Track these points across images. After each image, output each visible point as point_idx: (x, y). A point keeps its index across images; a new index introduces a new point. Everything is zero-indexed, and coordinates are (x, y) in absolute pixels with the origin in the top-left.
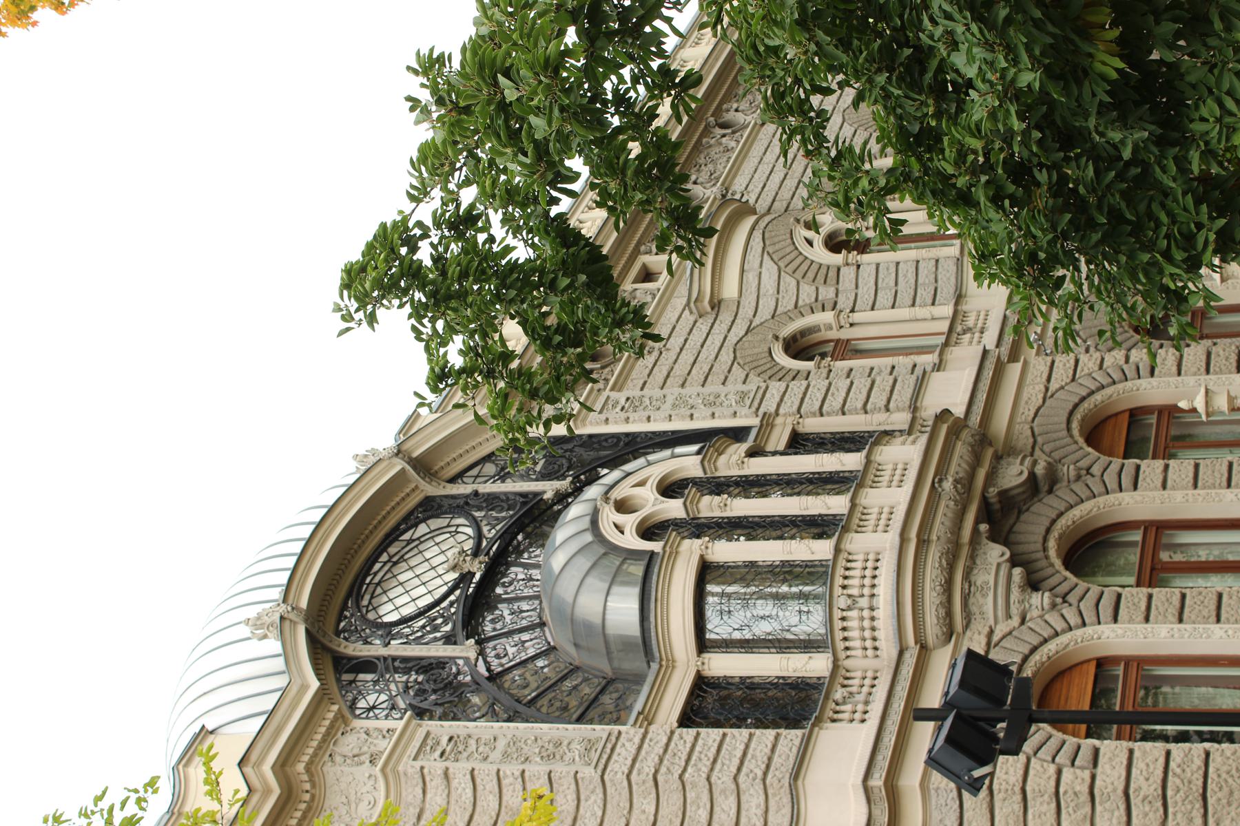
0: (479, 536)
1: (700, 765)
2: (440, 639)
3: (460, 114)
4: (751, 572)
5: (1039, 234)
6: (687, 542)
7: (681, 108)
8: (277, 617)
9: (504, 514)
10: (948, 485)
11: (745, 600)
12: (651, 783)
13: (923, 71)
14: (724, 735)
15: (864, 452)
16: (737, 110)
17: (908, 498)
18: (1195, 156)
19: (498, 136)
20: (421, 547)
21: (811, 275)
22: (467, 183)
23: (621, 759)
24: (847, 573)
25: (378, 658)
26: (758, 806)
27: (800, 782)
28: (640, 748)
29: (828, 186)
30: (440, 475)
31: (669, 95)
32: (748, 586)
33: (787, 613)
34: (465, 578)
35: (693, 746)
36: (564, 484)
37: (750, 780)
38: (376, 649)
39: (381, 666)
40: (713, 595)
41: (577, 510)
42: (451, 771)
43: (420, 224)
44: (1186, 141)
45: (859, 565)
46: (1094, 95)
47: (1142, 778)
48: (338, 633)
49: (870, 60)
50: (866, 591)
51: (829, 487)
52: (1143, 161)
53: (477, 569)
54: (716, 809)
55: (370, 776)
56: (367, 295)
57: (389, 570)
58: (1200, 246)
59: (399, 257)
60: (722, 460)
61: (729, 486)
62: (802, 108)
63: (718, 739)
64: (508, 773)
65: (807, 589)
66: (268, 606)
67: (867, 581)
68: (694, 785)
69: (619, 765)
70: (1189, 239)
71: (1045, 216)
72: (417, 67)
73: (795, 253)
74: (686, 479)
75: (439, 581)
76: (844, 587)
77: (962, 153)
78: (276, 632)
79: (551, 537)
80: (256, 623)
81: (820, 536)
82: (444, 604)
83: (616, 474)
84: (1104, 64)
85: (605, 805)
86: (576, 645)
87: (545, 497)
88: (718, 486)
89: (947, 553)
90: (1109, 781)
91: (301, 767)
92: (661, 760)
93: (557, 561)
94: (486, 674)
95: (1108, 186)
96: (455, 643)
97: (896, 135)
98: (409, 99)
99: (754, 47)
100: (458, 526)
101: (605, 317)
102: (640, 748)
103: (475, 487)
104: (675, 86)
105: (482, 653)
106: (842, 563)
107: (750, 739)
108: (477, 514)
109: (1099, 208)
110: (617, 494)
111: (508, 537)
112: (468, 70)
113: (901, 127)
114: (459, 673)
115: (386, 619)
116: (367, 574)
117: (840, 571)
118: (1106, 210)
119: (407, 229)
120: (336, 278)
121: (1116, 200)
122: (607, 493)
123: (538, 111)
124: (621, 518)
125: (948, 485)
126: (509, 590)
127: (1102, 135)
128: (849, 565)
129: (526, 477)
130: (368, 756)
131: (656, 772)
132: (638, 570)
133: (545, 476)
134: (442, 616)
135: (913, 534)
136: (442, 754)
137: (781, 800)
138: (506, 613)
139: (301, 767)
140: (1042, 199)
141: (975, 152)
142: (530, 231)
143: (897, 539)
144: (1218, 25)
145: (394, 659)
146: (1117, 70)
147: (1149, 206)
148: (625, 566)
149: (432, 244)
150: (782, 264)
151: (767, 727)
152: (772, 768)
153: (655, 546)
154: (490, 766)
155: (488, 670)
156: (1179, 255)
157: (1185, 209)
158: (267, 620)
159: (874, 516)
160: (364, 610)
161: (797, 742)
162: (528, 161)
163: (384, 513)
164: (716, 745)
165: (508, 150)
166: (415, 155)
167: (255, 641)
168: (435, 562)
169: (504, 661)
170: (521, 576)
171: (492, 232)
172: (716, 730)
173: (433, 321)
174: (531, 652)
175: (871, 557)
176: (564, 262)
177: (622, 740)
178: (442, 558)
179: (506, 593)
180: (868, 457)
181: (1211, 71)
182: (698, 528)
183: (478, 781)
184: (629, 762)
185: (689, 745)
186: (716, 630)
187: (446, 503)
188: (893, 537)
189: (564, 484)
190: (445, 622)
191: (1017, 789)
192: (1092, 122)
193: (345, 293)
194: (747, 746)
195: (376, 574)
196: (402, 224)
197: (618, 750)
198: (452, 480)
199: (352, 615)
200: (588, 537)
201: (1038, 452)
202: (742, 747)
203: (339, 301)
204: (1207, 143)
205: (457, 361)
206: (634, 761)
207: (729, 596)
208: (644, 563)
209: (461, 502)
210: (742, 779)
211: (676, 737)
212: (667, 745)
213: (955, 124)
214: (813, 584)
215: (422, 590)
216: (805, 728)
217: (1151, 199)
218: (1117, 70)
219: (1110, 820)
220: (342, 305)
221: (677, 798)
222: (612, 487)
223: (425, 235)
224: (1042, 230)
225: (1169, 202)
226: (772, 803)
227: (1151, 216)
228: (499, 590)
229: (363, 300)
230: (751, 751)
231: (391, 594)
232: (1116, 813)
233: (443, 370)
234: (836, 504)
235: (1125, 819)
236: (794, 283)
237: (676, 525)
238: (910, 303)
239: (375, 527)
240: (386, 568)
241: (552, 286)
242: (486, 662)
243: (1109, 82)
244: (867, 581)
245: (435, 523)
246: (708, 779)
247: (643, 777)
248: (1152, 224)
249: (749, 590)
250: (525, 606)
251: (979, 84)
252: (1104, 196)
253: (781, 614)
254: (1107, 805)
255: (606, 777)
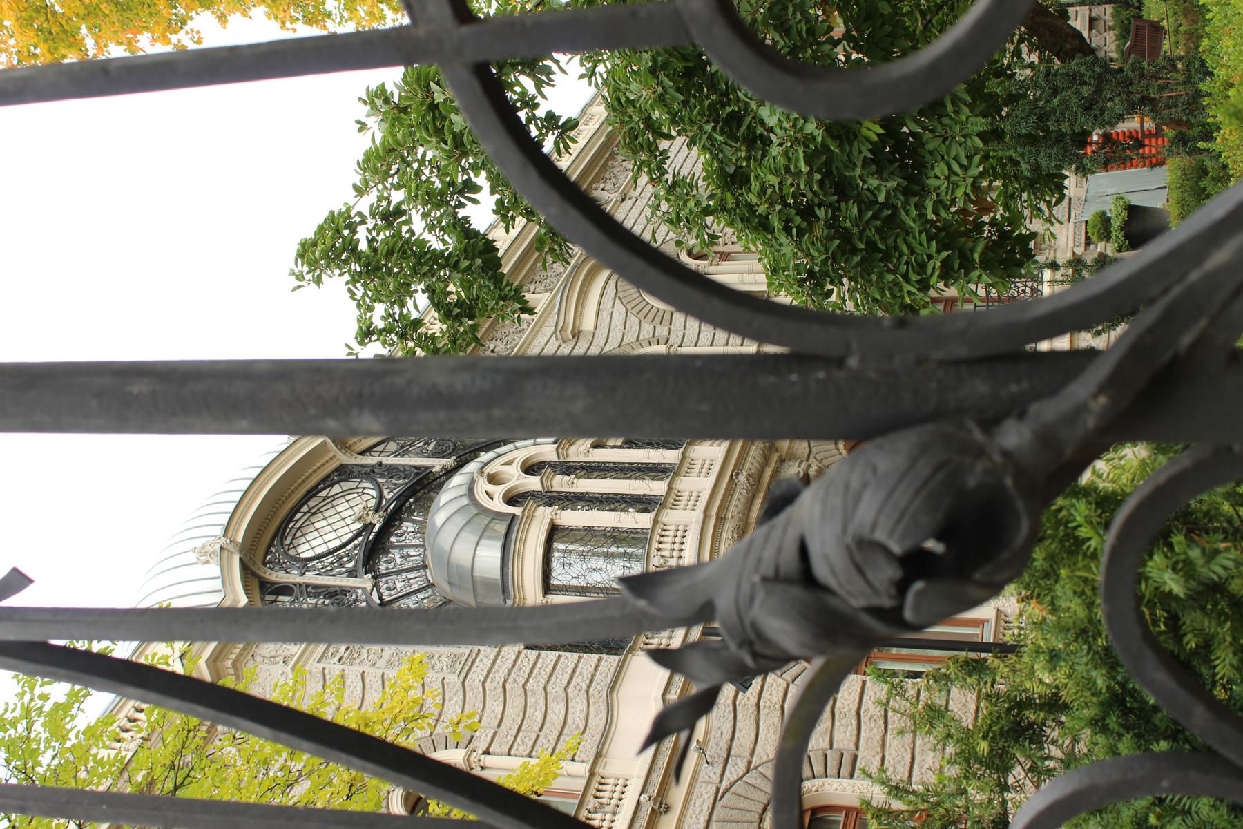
0: (381, 497)
1: (539, 678)
2: (344, 573)
3: (400, 112)
4: (588, 535)
5: (816, 254)
6: (541, 508)
7: (561, 145)
8: (218, 546)
9: (401, 481)
10: (742, 478)
11: (583, 556)
12: (501, 689)
13: (739, 126)
14: (560, 656)
15: (682, 450)
16: (603, 189)
17: (712, 486)
18: (929, 205)
19: (427, 129)
20: (335, 503)
21: (650, 316)
22: (397, 187)
23: (479, 670)
24: (662, 539)
25: (295, 585)
26: (581, 711)
27: (614, 694)
28: (494, 662)
29: (664, 206)
30: (353, 448)
31: (553, 134)
32: (585, 545)
33: (614, 567)
34: (368, 527)
35: (535, 663)
36: (450, 462)
37: (576, 691)
38: (294, 577)
39: (296, 590)
40: (558, 550)
41: (458, 479)
42: (346, 672)
43: (359, 214)
44: (924, 192)
45: (671, 533)
46: (860, 152)
47: (870, 702)
48: (265, 564)
49: (701, 114)
50: (675, 554)
51: (653, 474)
52: (893, 205)
53: (378, 522)
54: (549, 711)
55: (283, 673)
56: (316, 262)
57: (308, 518)
58: (929, 271)
59: (342, 236)
60: (573, 448)
61: (576, 469)
62: (651, 148)
63: (555, 659)
64: (391, 676)
65: (630, 550)
66: (211, 539)
67: (676, 546)
68: (534, 693)
69: (477, 674)
70: (922, 266)
71: (821, 242)
72: (366, 99)
73: (640, 299)
74: (544, 462)
75: (346, 530)
76: (659, 550)
77: (762, 191)
78: (216, 559)
79: (436, 500)
80: (202, 551)
81: (646, 510)
82: (349, 547)
83: (490, 455)
84: (869, 129)
85: (464, 705)
86: (449, 583)
87: (434, 470)
88: (568, 469)
89: (739, 528)
90: (846, 703)
91: (229, 663)
92: (510, 673)
93: (439, 518)
94: (379, 602)
95: (868, 222)
96: (356, 577)
97: (717, 177)
98: (358, 122)
99: (618, 100)
100: (364, 488)
101: (493, 292)
102: (494, 662)
103: (380, 459)
104: (558, 127)
105: (376, 585)
106: (658, 531)
107: (579, 661)
108: (380, 480)
109: (861, 240)
110: (490, 469)
111: (402, 499)
112: (408, 79)
113: (721, 169)
114: (356, 600)
115: (302, 556)
116: (290, 521)
117: (656, 538)
118: (865, 240)
119: (349, 217)
120: (294, 249)
121: (871, 233)
122: (482, 468)
123: (456, 111)
124: (491, 488)
125: (742, 478)
126: (401, 539)
127: (864, 182)
128: (663, 533)
129: (420, 454)
130: (282, 657)
131: (505, 681)
132: (501, 528)
133: (436, 454)
134: (348, 555)
135: (714, 512)
136: (340, 659)
137: (599, 708)
138: (397, 556)
139: (229, 663)
140: (820, 231)
141: (772, 186)
142: (442, 229)
143: (702, 515)
144: (950, 108)
145: (307, 586)
146: (878, 135)
147: (895, 241)
148: (492, 525)
149: (367, 229)
150: (629, 307)
151: (591, 652)
152: (594, 683)
153: (517, 510)
154: (377, 671)
155: (380, 598)
156: (914, 278)
157: (921, 244)
158: (210, 549)
159: (685, 498)
160: (287, 548)
161: (615, 665)
162: (447, 148)
163: (307, 474)
164: (552, 663)
165: (434, 139)
166: (361, 158)
167: (200, 566)
168: (344, 515)
169: (393, 592)
170: (411, 529)
171: (414, 227)
172: (553, 653)
173: (365, 285)
174: (415, 587)
175: (681, 528)
176: (465, 250)
177: (480, 656)
178: (350, 512)
179: (398, 541)
180: (683, 453)
181: (943, 142)
182: (550, 499)
183: (367, 681)
184: (485, 673)
185: (531, 663)
186: (559, 577)
187: (356, 470)
188: (698, 514)
189: (450, 462)
190: (349, 561)
191: (778, 707)
192: (858, 171)
193: (299, 261)
194: (576, 666)
195: (297, 521)
196: (346, 215)
197: (477, 663)
198: (362, 453)
199: (277, 551)
200: (465, 501)
201: (812, 459)
202: (573, 666)
203: (295, 268)
204: (938, 195)
205: (379, 324)
206: (489, 672)
207: (571, 552)
208: (508, 522)
209: (368, 470)
210: (570, 689)
211: (522, 655)
212: (515, 662)
213: (760, 165)
214: (635, 546)
215: (333, 535)
216: (621, 654)
217: (897, 236)
218: (878, 135)
219: (845, 732)
220: (296, 271)
221: (519, 703)
222: (487, 464)
223: (363, 222)
224: (819, 252)
225: (909, 238)
226: (592, 708)
227: (896, 248)
228: (393, 539)
229: (313, 265)
230: (579, 669)
231: (308, 537)
232: (850, 728)
233: (368, 329)
234: (657, 487)
235: (856, 732)
236: (638, 321)
237: (534, 496)
238: (725, 343)
239: (300, 485)
240: (306, 517)
241: (456, 266)
242: (379, 592)
243: (872, 143)
244: (676, 546)
245: (346, 485)
246: (545, 688)
247: (494, 684)
248: (897, 254)
249: (586, 549)
250: (412, 552)
251: (777, 130)
252: (864, 230)
253: (609, 567)
254: (844, 721)
255: (466, 683)
